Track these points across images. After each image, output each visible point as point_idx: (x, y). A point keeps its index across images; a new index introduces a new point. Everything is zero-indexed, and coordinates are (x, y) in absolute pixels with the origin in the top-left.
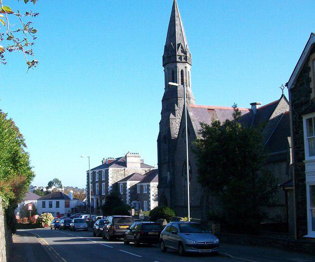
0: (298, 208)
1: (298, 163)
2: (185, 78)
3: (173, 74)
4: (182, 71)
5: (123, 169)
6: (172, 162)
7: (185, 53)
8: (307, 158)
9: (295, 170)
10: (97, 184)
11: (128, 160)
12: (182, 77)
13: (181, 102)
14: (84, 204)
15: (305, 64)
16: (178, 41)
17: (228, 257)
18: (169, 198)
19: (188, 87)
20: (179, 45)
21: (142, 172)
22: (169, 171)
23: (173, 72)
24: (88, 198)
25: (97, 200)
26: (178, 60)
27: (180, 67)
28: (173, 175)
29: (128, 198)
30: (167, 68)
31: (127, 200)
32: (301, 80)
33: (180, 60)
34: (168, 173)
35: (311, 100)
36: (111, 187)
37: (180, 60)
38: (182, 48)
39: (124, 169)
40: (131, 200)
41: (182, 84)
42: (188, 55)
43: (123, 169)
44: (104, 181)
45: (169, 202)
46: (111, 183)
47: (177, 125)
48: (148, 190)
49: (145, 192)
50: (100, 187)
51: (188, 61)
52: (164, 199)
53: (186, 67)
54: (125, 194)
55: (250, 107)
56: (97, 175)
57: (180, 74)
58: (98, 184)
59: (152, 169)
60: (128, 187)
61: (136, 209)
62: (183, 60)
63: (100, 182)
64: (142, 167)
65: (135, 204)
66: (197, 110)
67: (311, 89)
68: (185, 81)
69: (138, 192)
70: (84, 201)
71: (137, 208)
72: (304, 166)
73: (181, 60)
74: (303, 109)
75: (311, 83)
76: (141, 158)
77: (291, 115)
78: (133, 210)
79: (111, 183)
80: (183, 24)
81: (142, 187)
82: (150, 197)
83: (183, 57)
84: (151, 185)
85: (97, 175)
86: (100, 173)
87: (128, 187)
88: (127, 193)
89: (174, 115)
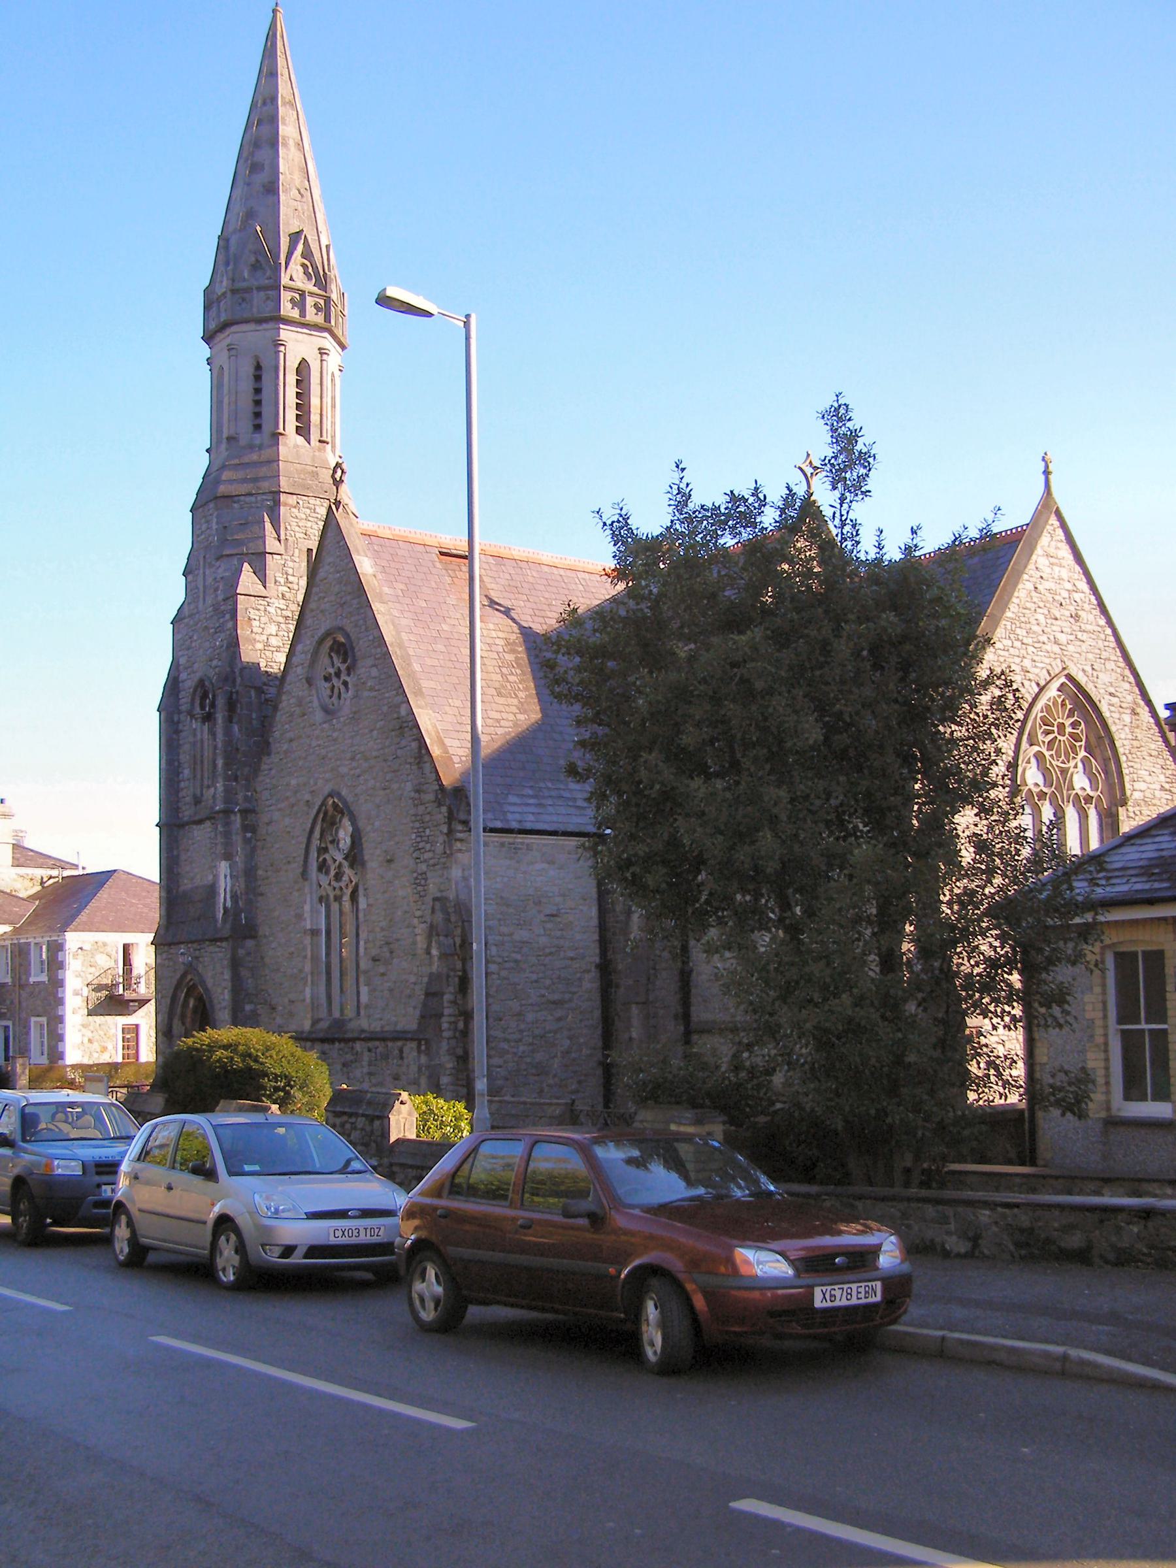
2: (315, 401)
3: (258, 378)
4: (303, 368)
6: (245, 812)
7: (322, 281)
12: (303, 396)
16: (289, 222)
20: (295, 237)
22: (228, 856)
23: (258, 367)
26: (287, 309)
28: (249, 874)
33: (295, 314)
34: (224, 867)
37: (295, 314)
38: (307, 254)
41: (303, 430)
48: (55, 964)
49: (38, 977)
53: (322, 352)
57: (292, 378)
59: (67, 873)
62: (312, 316)
64: (17, 863)
68: (315, 418)
73: (303, 313)
80: (312, 143)
82: (61, 1002)
83: (310, 301)
84: (68, 946)
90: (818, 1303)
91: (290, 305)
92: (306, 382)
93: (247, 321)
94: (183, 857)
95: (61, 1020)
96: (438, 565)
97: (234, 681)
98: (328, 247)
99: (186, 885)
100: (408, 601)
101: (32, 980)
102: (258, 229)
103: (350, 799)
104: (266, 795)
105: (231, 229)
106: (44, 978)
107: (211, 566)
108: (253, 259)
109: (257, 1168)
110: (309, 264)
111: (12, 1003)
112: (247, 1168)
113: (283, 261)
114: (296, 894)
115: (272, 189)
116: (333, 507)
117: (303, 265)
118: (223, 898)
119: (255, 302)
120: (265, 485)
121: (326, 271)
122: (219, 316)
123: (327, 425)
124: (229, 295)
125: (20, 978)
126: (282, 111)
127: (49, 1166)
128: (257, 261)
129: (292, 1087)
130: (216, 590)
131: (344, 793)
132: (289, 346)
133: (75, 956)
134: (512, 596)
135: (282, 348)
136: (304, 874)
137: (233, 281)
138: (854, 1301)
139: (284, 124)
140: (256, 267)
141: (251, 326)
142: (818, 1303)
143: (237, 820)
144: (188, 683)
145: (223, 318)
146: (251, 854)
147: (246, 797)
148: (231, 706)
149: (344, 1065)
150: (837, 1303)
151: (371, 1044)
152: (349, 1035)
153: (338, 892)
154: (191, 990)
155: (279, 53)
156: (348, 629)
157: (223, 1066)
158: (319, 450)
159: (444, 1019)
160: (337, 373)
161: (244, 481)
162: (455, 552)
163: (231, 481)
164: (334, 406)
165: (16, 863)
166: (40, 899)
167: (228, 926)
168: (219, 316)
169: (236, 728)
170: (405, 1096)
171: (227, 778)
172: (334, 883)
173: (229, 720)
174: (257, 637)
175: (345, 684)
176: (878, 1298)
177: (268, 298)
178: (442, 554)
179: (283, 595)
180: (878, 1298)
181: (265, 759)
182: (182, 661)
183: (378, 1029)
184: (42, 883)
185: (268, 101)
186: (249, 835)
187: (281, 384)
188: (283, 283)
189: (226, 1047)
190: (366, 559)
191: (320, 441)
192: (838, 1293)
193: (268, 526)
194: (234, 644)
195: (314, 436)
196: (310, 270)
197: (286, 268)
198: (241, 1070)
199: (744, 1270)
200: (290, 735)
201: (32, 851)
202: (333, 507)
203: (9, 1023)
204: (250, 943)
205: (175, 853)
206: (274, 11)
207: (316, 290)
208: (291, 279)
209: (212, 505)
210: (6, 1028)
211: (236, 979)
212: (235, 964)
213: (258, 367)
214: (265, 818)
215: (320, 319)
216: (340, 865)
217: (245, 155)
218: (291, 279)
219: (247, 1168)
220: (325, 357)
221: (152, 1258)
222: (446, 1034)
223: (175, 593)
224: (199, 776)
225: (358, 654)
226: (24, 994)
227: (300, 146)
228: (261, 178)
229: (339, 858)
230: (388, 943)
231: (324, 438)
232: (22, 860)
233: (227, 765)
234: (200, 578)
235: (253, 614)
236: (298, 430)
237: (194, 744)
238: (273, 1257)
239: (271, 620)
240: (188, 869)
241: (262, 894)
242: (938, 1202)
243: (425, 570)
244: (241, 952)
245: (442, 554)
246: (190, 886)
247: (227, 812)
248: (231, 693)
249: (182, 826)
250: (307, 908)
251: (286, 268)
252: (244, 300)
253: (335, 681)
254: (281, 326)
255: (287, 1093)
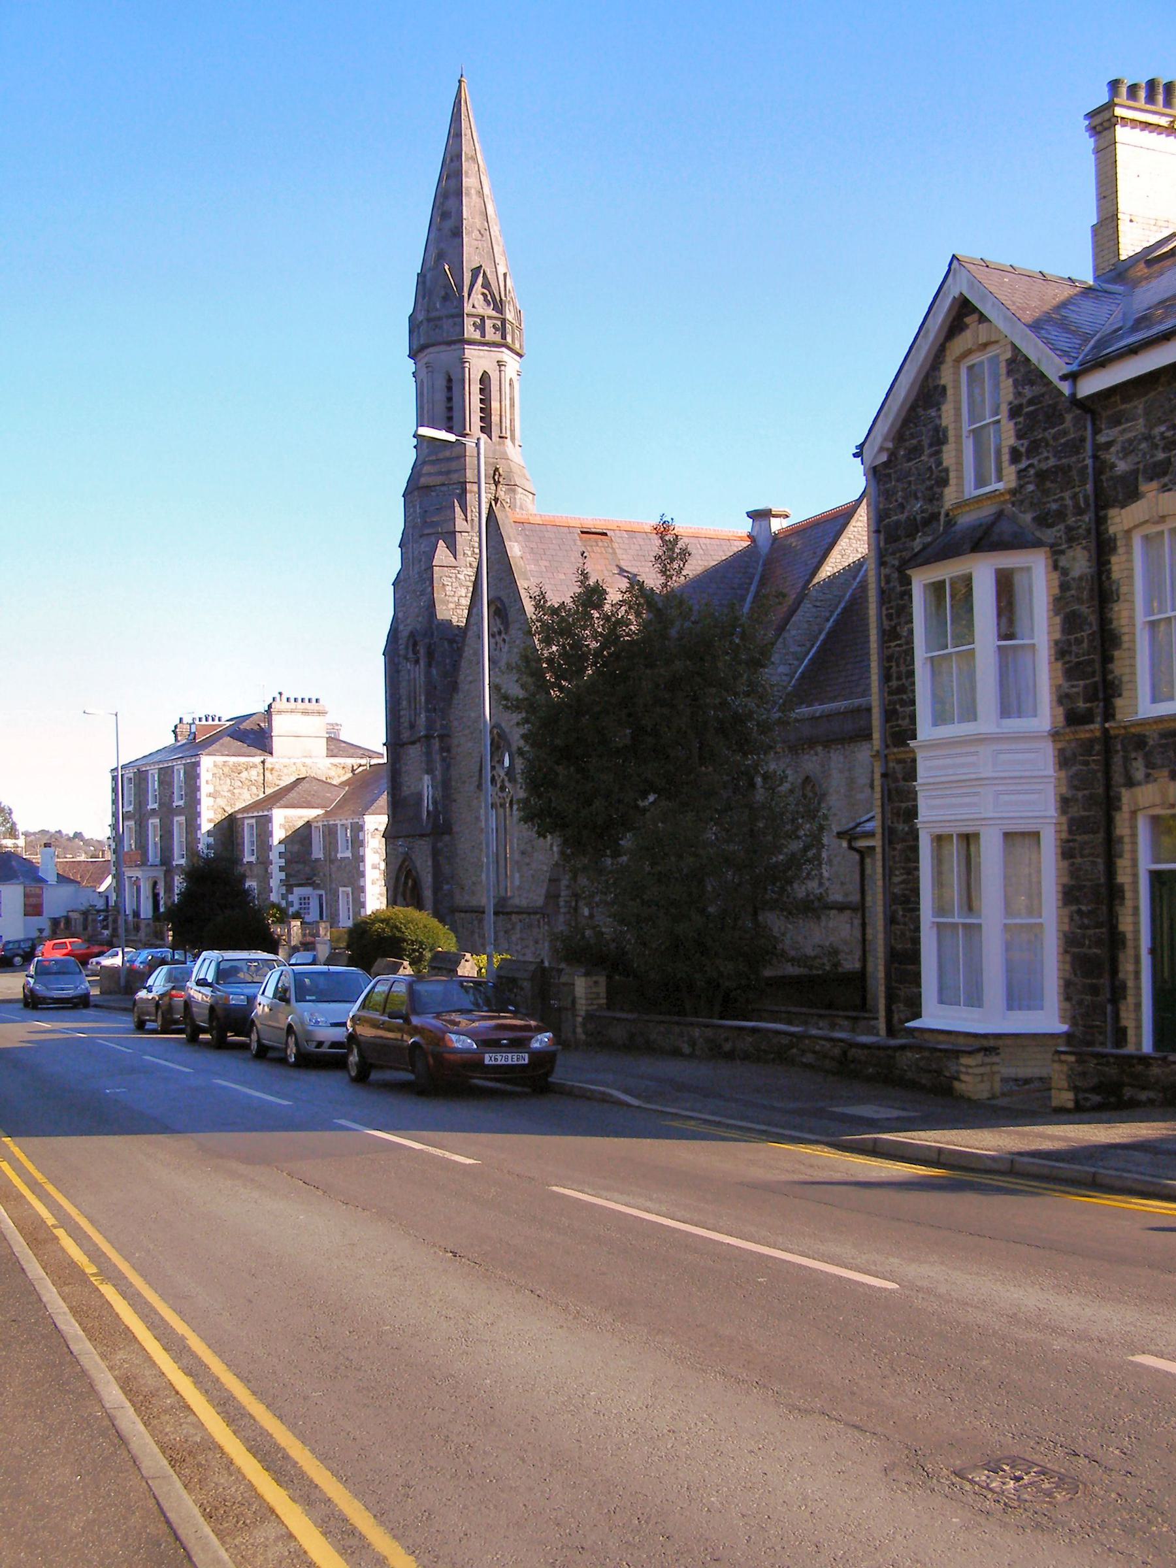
0: (891, 920)
1: (895, 750)
2: (495, 405)
4: (485, 379)
5: (262, 758)
6: (442, 737)
7: (499, 306)
8: (926, 730)
9: (884, 775)
10: (180, 819)
11: (280, 725)
12: (485, 401)
13: (481, 496)
14: (100, 904)
15: (927, 376)
16: (471, 257)
17: (605, 1099)
18: (427, 880)
19: (508, 442)
20: (476, 271)
21: (336, 771)
22: (430, 771)
23: (450, 380)
24: (118, 877)
25: (155, 884)
26: (470, 332)
27: (478, 360)
28: (446, 787)
29: (277, 877)
30: (428, 365)
31: (274, 883)
32: (912, 436)
33: (477, 335)
35: (943, 511)
36: (209, 833)
37: (477, 335)
38: (486, 285)
39: (263, 762)
40: (289, 886)
41: (486, 429)
42: (510, 316)
43: (257, 760)
44: (179, 811)
45: (428, 894)
46: (208, 818)
47: (463, 592)
49: (344, 853)
50: (167, 834)
51: (509, 339)
52: (410, 883)
53: (500, 364)
54: (265, 862)
55: (746, 526)
56: (154, 784)
57: (476, 387)
58: (182, 819)
59: (374, 761)
60: (278, 834)
61: (308, 919)
62: (491, 335)
63: (167, 811)
64: (331, 754)
65: (304, 900)
66: (528, 528)
67: (947, 470)
68: (495, 419)
69: (318, 853)
70: (102, 888)
71: (313, 916)
72: (914, 760)
73: (483, 335)
74: (917, 544)
75: (945, 448)
76: (330, 718)
77: (871, 565)
78: (296, 924)
79: (208, 818)
80: (493, 187)
81: (330, 832)
82: (362, 875)
83: (489, 323)
84: (366, 827)
85: (154, 784)
86: (166, 775)
87: (278, 834)
88: (274, 856)
89: (452, 548)
90: (487, 1062)
91: (472, 329)
92: (488, 390)
93: (439, 344)
94: (404, 769)
95: (362, 889)
96: (579, 543)
97: (432, 635)
98: (505, 275)
99: (406, 792)
100: (550, 575)
101: (339, 856)
102: (447, 267)
103: (507, 730)
104: (456, 723)
105: (428, 266)
106: (348, 854)
107: (417, 542)
108: (443, 293)
109: (314, 998)
110: (487, 293)
111: (325, 875)
112: (308, 998)
113: (466, 294)
114: (475, 801)
115: (457, 233)
116: (493, 503)
117: (483, 294)
118: (427, 803)
119: (445, 327)
120: (455, 477)
121: (503, 298)
122: (419, 340)
123: (506, 423)
124: (425, 323)
125: (330, 855)
126: (465, 165)
127: (227, 999)
128: (447, 294)
129: (424, 949)
130: (420, 561)
131: (503, 725)
132: (473, 361)
133: (373, 837)
134: (638, 564)
135: (467, 365)
136: (479, 786)
137: (428, 311)
138: (510, 1062)
139: (467, 177)
140: (446, 298)
141: (443, 348)
142: (487, 1062)
143: (436, 744)
144: (404, 634)
145: (422, 342)
146: (447, 767)
147: (442, 725)
148: (430, 654)
149: (506, 932)
150: (499, 1062)
151: (520, 917)
152: (509, 910)
153: (502, 801)
154: (409, 874)
155: (463, 117)
156: (505, 600)
157: (379, 935)
158: (499, 444)
159: (561, 899)
160: (515, 378)
161: (441, 473)
162: (593, 530)
163: (430, 474)
164: (512, 405)
165: (330, 754)
166: (349, 785)
167: (430, 826)
168: (419, 340)
169: (434, 671)
170: (468, 956)
171: (427, 710)
172: (500, 794)
173: (429, 665)
174: (450, 599)
175: (504, 640)
176: (526, 1062)
177: (455, 324)
178: (583, 532)
179: (470, 564)
180: (526, 1062)
181: (455, 695)
182: (400, 615)
183: (525, 905)
184: (353, 771)
185: (455, 159)
186: (445, 754)
187: (467, 394)
188: (466, 311)
189: (382, 921)
190: (516, 544)
191: (500, 437)
192: (499, 1058)
193: (458, 509)
194: (432, 605)
195: (495, 433)
196: (489, 298)
197: (469, 295)
198: (390, 937)
199: (450, 1044)
200: (470, 678)
201: (345, 742)
202: (493, 503)
203: (322, 892)
204: (447, 838)
205: (398, 766)
206: (460, 81)
207: (494, 314)
208: (473, 307)
209: (416, 493)
210: (321, 896)
211: (436, 866)
212: (435, 854)
213: (450, 380)
214: (455, 742)
215: (497, 338)
216: (503, 781)
217: (437, 204)
218: (473, 307)
219: (308, 998)
220: (503, 368)
221: (270, 1054)
222: (562, 910)
223: (394, 564)
224: (413, 707)
225: (510, 619)
226: (334, 869)
227: (481, 193)
228: (450, 224)
229: (502, 774)
230: (531, 841)
231: (503, 435)
232: (335, 751)
233: (427, 701)
234: (410, 550)
235: (446, 581)
236: (482, 429)
237: (409, 681)
238: (311, 1048)
239: (461, 585)
240: (407, 779)
241: (455, 801)
242: (678, 1023)
243: (568, 548)
244: (440, 845)
245: (583, 532)
246: (408, 793)
247: (428, 737)
248: (430, 645)
249: (403, 745)
250: (482, 812)
251: (469, 295)
252: (436, 326)
253: (497, 637)
254: (466, 346)
255: (421, 953)
